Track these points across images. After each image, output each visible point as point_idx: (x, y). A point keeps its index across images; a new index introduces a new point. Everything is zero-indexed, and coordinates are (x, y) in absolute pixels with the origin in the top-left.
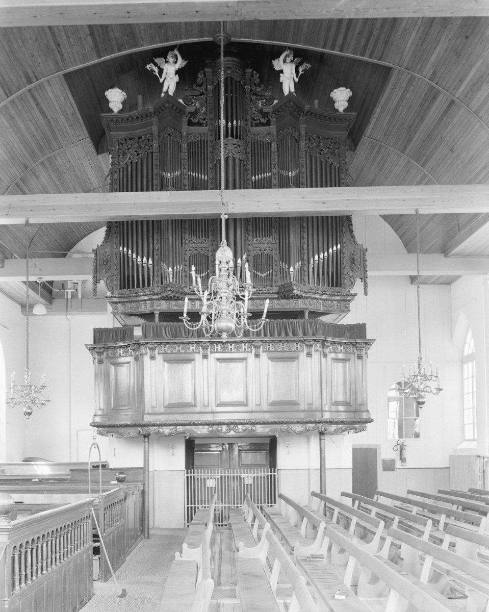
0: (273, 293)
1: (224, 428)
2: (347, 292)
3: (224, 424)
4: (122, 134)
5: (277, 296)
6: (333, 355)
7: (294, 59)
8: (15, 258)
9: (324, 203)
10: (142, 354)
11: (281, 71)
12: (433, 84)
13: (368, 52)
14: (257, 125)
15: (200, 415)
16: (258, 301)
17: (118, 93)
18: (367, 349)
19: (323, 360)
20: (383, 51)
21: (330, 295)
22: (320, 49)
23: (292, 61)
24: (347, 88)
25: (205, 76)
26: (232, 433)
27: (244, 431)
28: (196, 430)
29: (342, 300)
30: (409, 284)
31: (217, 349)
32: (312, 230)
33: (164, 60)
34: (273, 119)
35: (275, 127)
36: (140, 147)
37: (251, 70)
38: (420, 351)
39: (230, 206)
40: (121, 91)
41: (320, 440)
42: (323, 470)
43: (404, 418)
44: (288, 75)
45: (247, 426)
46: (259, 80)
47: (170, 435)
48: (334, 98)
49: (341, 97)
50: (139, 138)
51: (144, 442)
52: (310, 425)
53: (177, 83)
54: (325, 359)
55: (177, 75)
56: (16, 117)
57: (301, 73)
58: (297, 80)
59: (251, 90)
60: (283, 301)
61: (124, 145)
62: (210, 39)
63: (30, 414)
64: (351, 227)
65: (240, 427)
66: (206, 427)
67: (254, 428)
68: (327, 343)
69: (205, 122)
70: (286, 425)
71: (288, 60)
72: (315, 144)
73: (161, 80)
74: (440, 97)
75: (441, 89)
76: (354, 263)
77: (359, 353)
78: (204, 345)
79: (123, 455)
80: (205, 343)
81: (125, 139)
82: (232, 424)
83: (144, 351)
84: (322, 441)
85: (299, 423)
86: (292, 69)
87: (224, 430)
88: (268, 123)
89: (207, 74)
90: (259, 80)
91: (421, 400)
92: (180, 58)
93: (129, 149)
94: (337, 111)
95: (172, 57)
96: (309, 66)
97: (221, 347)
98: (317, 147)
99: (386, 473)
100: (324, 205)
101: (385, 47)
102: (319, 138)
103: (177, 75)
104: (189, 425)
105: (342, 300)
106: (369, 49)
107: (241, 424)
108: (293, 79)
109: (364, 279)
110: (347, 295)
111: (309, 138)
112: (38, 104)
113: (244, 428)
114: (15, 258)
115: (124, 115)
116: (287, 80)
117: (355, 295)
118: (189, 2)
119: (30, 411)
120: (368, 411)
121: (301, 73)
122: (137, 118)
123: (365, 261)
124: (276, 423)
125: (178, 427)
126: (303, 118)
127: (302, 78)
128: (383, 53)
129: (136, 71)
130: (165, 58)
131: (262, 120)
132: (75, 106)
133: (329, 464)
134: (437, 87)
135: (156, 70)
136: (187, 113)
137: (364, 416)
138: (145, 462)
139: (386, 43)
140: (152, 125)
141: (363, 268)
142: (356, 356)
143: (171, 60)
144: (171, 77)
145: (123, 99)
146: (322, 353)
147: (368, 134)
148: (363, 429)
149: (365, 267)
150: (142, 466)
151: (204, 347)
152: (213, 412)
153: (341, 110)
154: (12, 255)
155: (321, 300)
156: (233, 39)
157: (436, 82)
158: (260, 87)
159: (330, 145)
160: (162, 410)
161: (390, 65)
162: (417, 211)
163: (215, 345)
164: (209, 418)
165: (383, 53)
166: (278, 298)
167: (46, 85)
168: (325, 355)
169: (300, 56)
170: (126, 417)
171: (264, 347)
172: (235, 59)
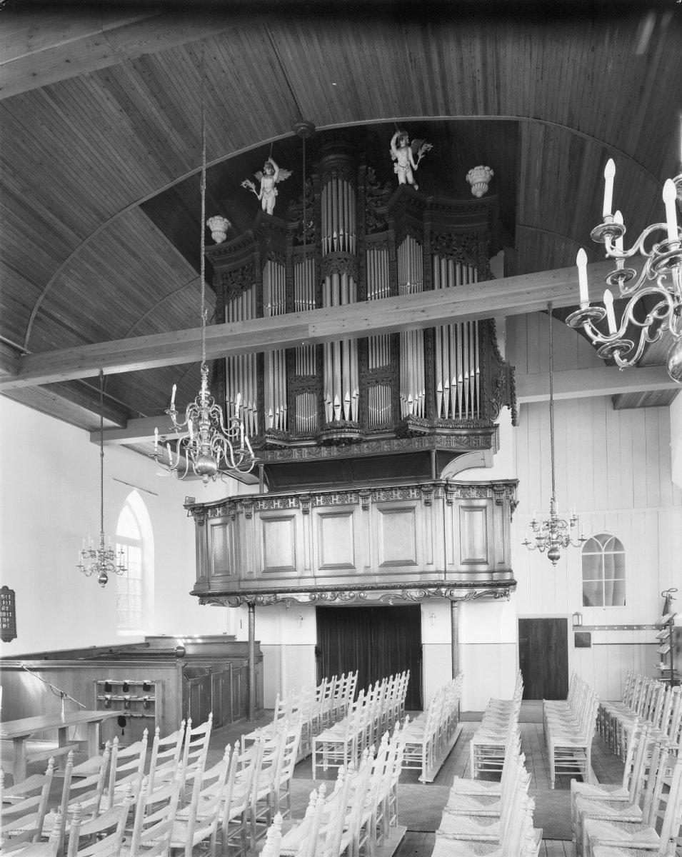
0: (390, 432)
1: (329, 595)
2: (488, 424)
3: (327, 590)
4: (226, 267)
5: (395, 435)
6: (463, 503)
7: (410, 141)
8: (142, 417)
9: (423, 311)
10: (238, 513)
11: (396, 161)
12: (574, 131)
13: (481, 107)
14: (373, 232)
15: (301, 580)
16: (374, 443)
17: (219, 222)
18: (509, 492)
19: (448, 509)
20: (499, 99)
21: (474, 428)
22: (421, 118)
23: (409, 145)
24: (485, 165)
25: (312, 184)
26: (338, 600)
27: (352, 597)
28: (297, 598)
29: (472, 435)
30: (610, 409)
31: (292, 505)
32: (440, 347)
33: (261, 173)
34: (391, 221)
35: (393, 230)
36: (244, 279)
37: (365, 167)
38: (553, 490)
39: (311, 329)
40: (221, 218)
41: (452, 607)
42: (455, 645)
43: (604, 580)
44: (404, 162)
45: (354, 592)
46: (374, 177)
47: (269, 604)
48: (471, 181)
49: (479, 178)
50: (244, 268)
51: (249, 612)
52: (431, 590)
53: (276, 197)
54: (450, 508)
55: (275, 188)
56: (102, 261)
57: (420, 157)
58: (415, 167)
59: (366, 191)
60: (404, 441)
61: (229, 279)
62: (292, 133)
63: (105, 582)
64: (494, 341)
65: (347, 593)
66: (309, 594)
67: (362, 594)
68: (451, 487)
69: (312, 238)
70: (401, 590)
71: (403, 143)
72: (444, 244)
73: (259, 197)
74: (588, 146)
75: (585, 136)
76: (497, 387)
77: (498, 497)
78: (304, 498)
79: (227, 621)
80: (304, 495)
81: (230, 273)
82: (336, 590)
83: (239, 509)
84: (454, 609)
85: (415, 587)
86: (408, 154)
87: (329, 598)
88: (386, 228)
89: (314, 181)
90: (374, 177)
91: (553, 554)
92: (276, 167)
93: (233, 283)
94: (475, 197)
95: (269, 168)
96: (430, 146)
97: (323, 500)
98: (448, 247)
99: (579, 649)
100: (423, 314)
101: (499, 94)
102: (450, 236)
103: (275, 188)
104: (288, 592)
105: (472, 435)
106: (480, 103)
107: (346, 590)
108: (411, 165)
109: (511, 404)
110: (489, 427)
111: (437, 237)
112: (123, 244)
113: (352, 595)
114: (142, 417)
115: (229, 243)
116: (402, 169)
117: (497, 426)
118: (665, 209)
119: (105, 579)
120: (511, 571)
121: (420, 157)
122: (239, 246)
123: (512, 381)
124: (387, 588)
125: (278, 595)
126: (426, 214)
127: (421, 165)
128: (499, 104)
129: (231, 189)
130: (263, 171)
131: (379, 225)
132: (168, 241)
133: (463, 638)
134: (580, 134)
135: (253, 186)
136: (290, 231)
137: (508, 576)
138: (250, 636)
139: (498, 87)
140: (254, 251)
141: (509, 392)
142: (495, 502)
143: (268, 171)
144: (268, 191)
145: (226, 228)
146: (446, 501)
147: (522, 222)
148: (505, 594)
149: (513, 388)
150: (247, 640)
151: (303, 500)
152: (315, 577)
153: (479, 194)
154: (138, 415)
155: (452, 435)
156: (318, 128)
157: (577, 127)
158: (377, 185)
159: (466, 242)
160: (260, 575)
161: (514, 118)
162: (550, 304)
163: (317, 498)
164: (310, 583)
165: (499, 104)
166: (395, 438)
167: (123, 219)
168: (450, 503)
169: (416, 132)
170: (217, 586)
171: (373, 497)
172: (343, 156)
